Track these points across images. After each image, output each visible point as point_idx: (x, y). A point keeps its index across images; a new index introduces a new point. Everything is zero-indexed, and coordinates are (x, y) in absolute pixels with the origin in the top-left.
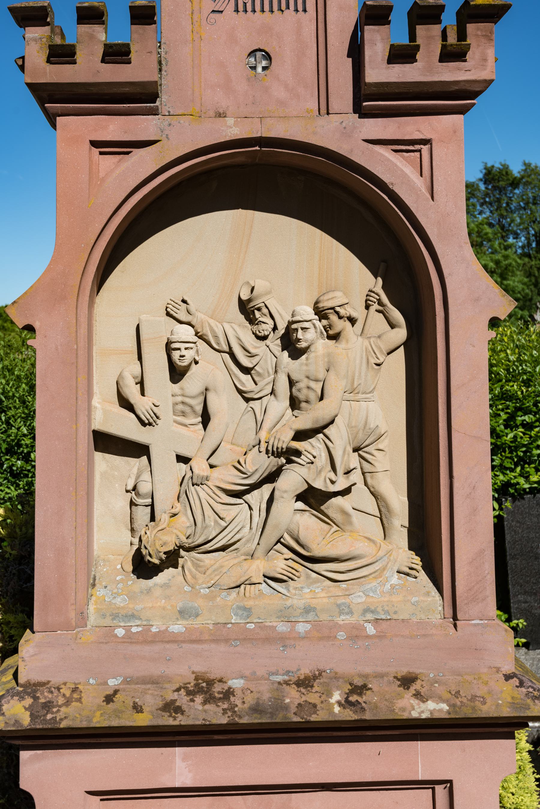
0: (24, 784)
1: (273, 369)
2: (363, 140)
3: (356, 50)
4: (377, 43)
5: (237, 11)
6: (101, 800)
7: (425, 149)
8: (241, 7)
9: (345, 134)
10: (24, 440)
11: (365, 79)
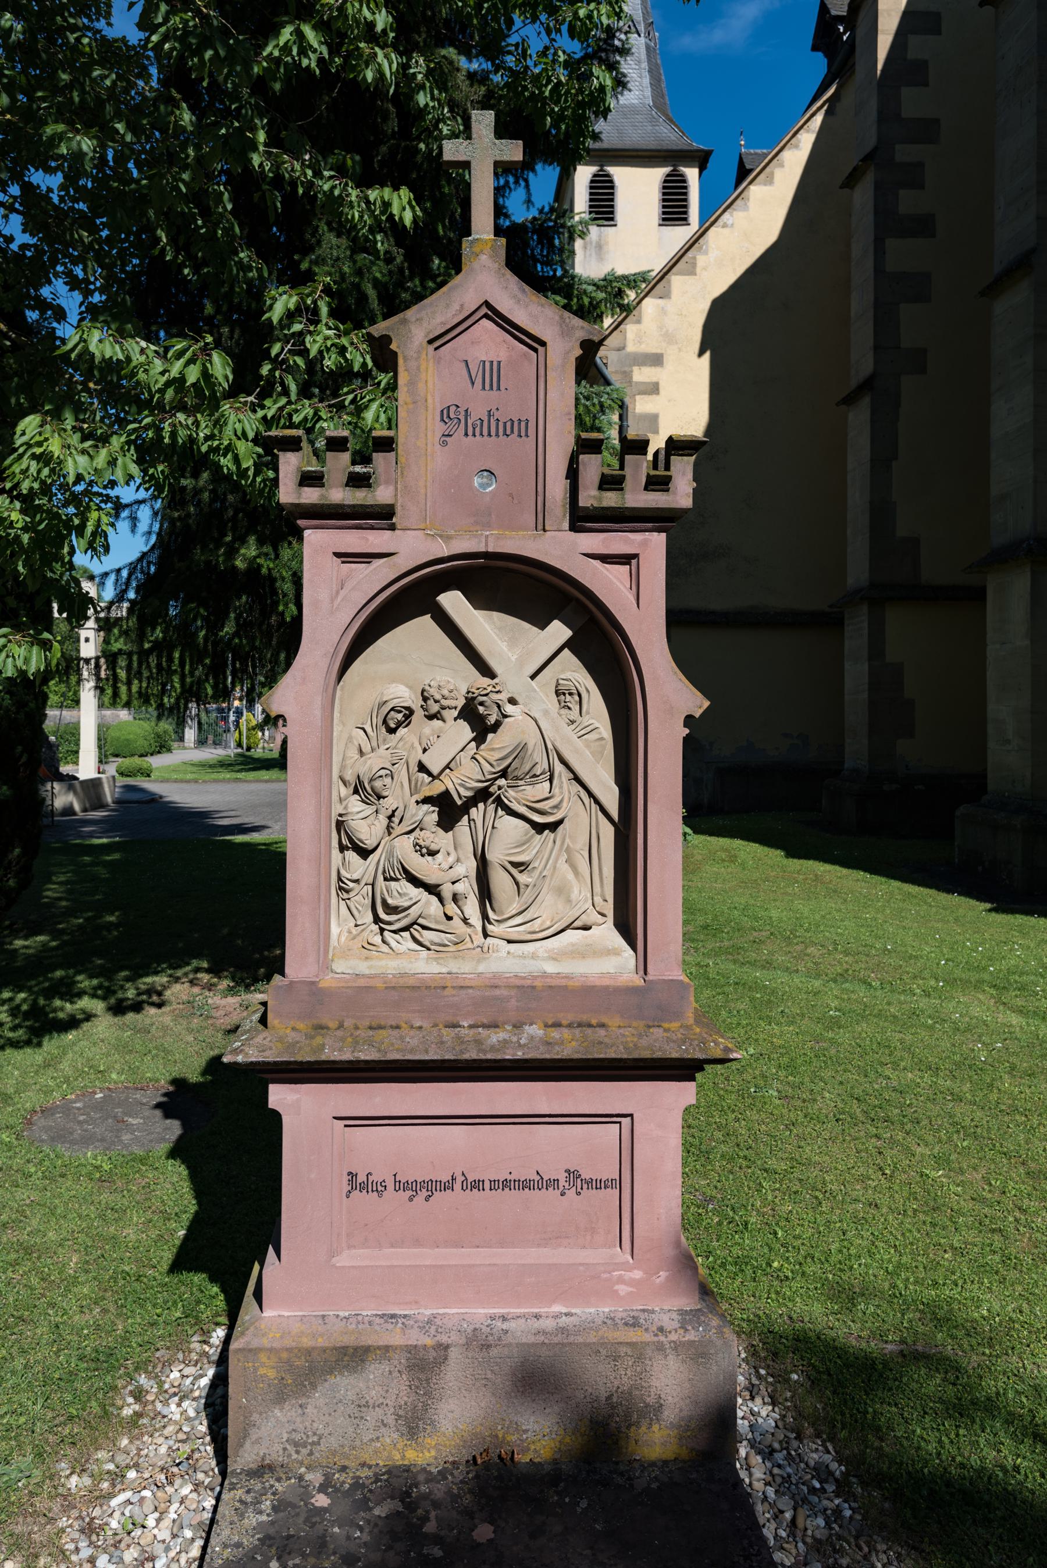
0: (271, 1105)
2: (584, 554)
3: (573, 474)
4: (592, 467)
5: (466, 435)
6: (346, 1126)
7: (625, 1121)
8: (470, 432)
9: (565, 550)
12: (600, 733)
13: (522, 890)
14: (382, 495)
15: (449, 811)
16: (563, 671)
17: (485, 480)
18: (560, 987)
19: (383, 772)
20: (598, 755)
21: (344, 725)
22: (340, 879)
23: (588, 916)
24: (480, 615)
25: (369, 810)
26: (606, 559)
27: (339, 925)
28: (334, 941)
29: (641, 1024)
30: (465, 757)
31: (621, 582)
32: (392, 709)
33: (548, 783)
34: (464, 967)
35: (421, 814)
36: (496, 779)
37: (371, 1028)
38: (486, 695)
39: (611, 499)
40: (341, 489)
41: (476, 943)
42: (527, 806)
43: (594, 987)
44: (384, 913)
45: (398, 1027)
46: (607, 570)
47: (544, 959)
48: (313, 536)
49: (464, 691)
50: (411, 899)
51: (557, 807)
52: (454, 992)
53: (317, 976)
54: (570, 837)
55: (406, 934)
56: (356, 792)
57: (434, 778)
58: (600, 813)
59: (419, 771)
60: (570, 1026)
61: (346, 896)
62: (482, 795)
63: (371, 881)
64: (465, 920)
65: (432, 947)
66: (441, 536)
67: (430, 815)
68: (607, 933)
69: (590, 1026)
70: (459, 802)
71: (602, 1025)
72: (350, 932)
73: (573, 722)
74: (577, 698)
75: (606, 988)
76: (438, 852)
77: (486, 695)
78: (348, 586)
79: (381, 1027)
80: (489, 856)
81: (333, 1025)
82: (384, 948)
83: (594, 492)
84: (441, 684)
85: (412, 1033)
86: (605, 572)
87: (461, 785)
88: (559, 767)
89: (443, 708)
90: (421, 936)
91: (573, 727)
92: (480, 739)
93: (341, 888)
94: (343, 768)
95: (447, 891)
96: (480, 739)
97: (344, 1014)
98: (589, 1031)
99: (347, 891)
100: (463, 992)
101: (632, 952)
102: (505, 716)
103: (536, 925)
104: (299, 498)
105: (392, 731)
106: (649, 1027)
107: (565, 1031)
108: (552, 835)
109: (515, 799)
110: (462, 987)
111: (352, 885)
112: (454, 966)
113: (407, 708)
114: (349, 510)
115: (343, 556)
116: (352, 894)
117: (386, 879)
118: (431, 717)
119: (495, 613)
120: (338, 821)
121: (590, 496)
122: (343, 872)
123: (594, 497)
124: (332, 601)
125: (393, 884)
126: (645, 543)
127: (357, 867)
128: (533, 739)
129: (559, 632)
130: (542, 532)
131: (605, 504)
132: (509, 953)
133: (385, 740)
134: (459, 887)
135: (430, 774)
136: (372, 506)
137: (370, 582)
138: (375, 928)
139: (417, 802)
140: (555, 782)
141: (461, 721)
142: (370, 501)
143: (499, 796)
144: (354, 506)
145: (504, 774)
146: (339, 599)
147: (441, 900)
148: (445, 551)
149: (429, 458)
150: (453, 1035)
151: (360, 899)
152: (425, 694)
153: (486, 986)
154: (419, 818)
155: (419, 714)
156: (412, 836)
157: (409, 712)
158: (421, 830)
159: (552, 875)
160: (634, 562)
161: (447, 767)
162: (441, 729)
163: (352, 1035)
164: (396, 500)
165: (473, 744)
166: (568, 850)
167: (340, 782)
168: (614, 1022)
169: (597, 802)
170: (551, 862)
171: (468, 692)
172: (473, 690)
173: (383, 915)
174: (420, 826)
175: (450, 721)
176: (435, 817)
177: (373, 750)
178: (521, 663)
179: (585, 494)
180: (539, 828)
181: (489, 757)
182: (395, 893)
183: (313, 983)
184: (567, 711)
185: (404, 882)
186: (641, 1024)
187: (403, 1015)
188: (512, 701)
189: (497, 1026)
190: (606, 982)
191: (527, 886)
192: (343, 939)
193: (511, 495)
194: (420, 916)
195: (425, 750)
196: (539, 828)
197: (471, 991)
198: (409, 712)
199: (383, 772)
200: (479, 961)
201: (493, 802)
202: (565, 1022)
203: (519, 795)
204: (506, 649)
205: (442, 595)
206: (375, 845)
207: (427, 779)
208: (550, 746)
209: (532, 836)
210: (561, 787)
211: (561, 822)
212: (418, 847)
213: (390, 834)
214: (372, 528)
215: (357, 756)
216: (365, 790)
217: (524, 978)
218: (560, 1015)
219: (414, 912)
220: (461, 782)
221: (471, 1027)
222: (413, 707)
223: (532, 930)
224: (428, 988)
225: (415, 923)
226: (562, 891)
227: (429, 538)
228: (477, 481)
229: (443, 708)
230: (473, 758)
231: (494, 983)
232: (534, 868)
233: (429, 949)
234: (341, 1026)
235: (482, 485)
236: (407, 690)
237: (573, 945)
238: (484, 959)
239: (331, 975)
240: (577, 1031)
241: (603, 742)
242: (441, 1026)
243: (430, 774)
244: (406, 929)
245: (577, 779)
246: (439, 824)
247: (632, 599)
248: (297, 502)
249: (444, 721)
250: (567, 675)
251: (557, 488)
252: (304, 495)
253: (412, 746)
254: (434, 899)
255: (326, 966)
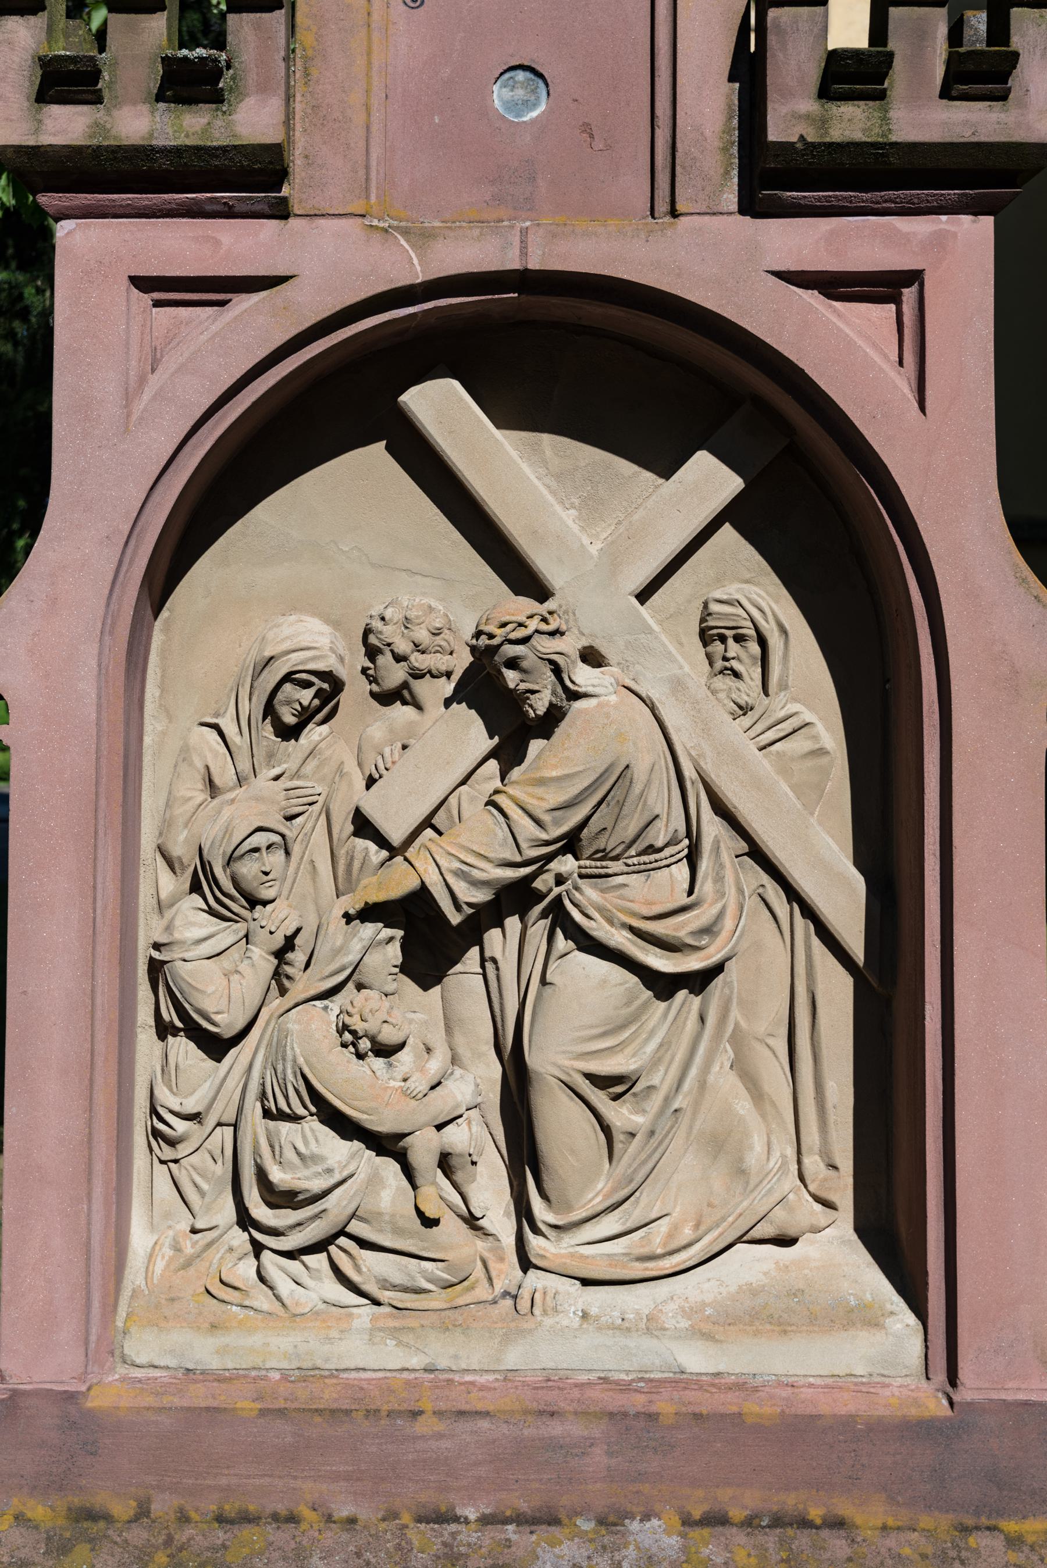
1: (301, 663)
2: (779, 275)
3: (749, 70)
9: (728, 263)
10: (581, 1557)
11: (766, 136)
12: (816, 738)
13: (618, 1146)
14: (251, 120)
15: (430, 939)
16: (719, 581)
17: (520, 93)
18: (723, 1416)
19: (260, 839)
20: (810, 792)
21: (170, 718)
22: (154, 1111)
23: (791, 1210)
24: (509, 443)
25: (228, 934)
26: (836, 286)
27: (152, 1227)
28: (134, 1275)
29: (942, 1522)
30: (471, 801)
31: (874, 345)
32: (288, 678)
33: (682, 871)
34: (472, 1354)
35: (356, 948)
36: (549, 858)
37: (221, 1519)
38: (525, 641)
39: (851, 122)
40: (145, 108)
41: (499, 1287)
42: (632, 929)
43: (814, 1418)
44: (263, 1203)
45: (292, 1519)
46: (839, 315)
47: (680, 1336)
48: (78, 236)
49: (468, 632)
50: (329, 1171)
51: (708, 931)
52: (441, 1427)
53: (82, 1378)
54: (741, 1003)
55: (318, 1261)
56: (195, 887)
57: (393, 851)
58: (816, 942)
59: (356, 834)
60: (749, 1523)
61: (168, 1153)
62: (514, 898)
63: (230, 1116)
64: (472, 1221)
65: (384, 1296)
66: (406, 232)
67: (383, 948)
68: (837, 1256)
69: (805, 1523)
70: (455, 919)
71: (838, 1524)
72: (177, 1249)
73: (745, 709)
74: (755, 648)
75: (847, 1423)
76: (402, 1046)
77: (525, 641)
78: (170, 363)
79: (247, 1518)
80: (533, 1059)
81: (122, 1509)
82: (262, 1299)
83: (809, 105)
84: (412, 614)
85: (331, 1537)
86: (834, 319)
87: (460, 874)
88: (712, 827)
89: (417, 675)
90: (357, 1268)
91: (746, 721)
92: (509, 753)
93: (156, 1133)
94: (166, 825)
95: (423, 1148)
96: (509, 753)
97: (151, 1480)
98: (803, 1540)
99: (172, 1143)
100: (464, 1427)
101: (911, 1319)
102: (574, 696)
103: (657, 1237)
104: (37, 131)
105: (289, 733)
106: (965, 1530)
107: (739, 1537)
108: (696, 1001)
109: (600, 910)
110: (461, 1413)
111: (181, 1126)
112: (442, 1351)
113: (325, 676)
114: (165, 164)
115: (162, 288)
116: (183, 1150)
117: (267, 1114)
118: (386, 698)
119: (546, 438)
120: (152, 961)
121: (798, 117)
122: (166, 1097)
123: (807, 117)
124: (129, 397)
125: (285, 1127)
126: (940, 240)
127: (193, 1079)
128: (646, 756)
129: (709, 480)
130: (668, 219)
131: (836, 135)
132: (585, 1316)
133: (270, 756)
134: (456, 1137)
135: (382, 842)
136: (224, 149)
137: (220, 351)
138: (240, 1238)
139: (348, 918)
140: (705, 865)
141: (460, 709)
142: (219, 138)
143: (559, 898)
144: (178, 152)
145: (570, 843)
146: (146, 397)
147: (408, 1172)
148: (417, 270)
149: (376, 36)
150: (437, 1547)
151: (205, 1164)
152: (372, 639)
153: (526, 1412)
154: (353, 957)
155: (355, 692)
156: (334, 1005)
157: (331, 688)
158: (360, 987)
159: (697, 1104)
160: (909, 294)
161: (428, 822)
162: (411, 728)
163: (169, 1541)
164: (288, 137)
165: (493, 765)
166: (738, 1040)
167: (160, 859)
168: (869, 1514)
169: (809, 912)
170: (693, 1072)
171: (478, 634)
172: (491, 628)
173: (260, 1212)
174: (354, 979)
175: (435, 709)
176: (394, 953)
177: (240, 781)
178: (614, 559)
179: (784, 110)
180: (663, 986)
181: (531, 803)
182: (290, 1155)
183: (70, 1397)
184: (729, 681)
185: (313, 1126)
186: (942, 1522)
187: (308, 1485)
188: (592, 657)
189: (554, 1521)
190: (847, 1405)
191: (633, 1135)
192: (160, 1266)
193: (587, 129)
194: (353, 1215)
195: (371, 782)
196: (663, 986)
197: (484, 1424)
198: (331, 688)
199: (260, 839)
200: (507, 1339)
201: (544, 915)
202: (737, 1514)
203: (609, 900)
204: (575, 528)
205: (414, 390)
206: (240, 1024)
207: (376, 854)
208: (689, 772)
209: (645, 1006)
210: (719, 879)
211: (718, 969)
212: (349, 1036)
213: (283, 991)
214: (229, 213)
215: (201, 796)
216: (222, 887)
217: (625, 1387)
218: (725, 1494)
219: (337, 1205)
220: (460, 866)
221: (485, 1521)
222: (342, 672)
223: (645, 1251)
224: (372, 1413)
225: (342, 1233)
226: (722, 1145)
227: (377, 236)
228: (499, 95)
229: (417, 675)
230: (491, 803)
231: (549, 1399)
232: (651, 1088)
233: (377, 1303)
234: (143, 1512)
235: (512, 106)
236: (327, 629)
237: (754, 1292)
238: (522, 1333)
239: (122, 1370)
240: (770, 1540)
241: (824, 760)
242: (406, 1518)
243: (382, 842)
244: (318, 1247)
245: (757, 854)
246: (405, 969)
247: (903, 385)
248: (32, 143)
249: (419, 707)
250: (732, 590)
251: (708, 104)
252: (49, 124)
253: (340, 771)
254: (390, 1167)
255: (102, 1346)
